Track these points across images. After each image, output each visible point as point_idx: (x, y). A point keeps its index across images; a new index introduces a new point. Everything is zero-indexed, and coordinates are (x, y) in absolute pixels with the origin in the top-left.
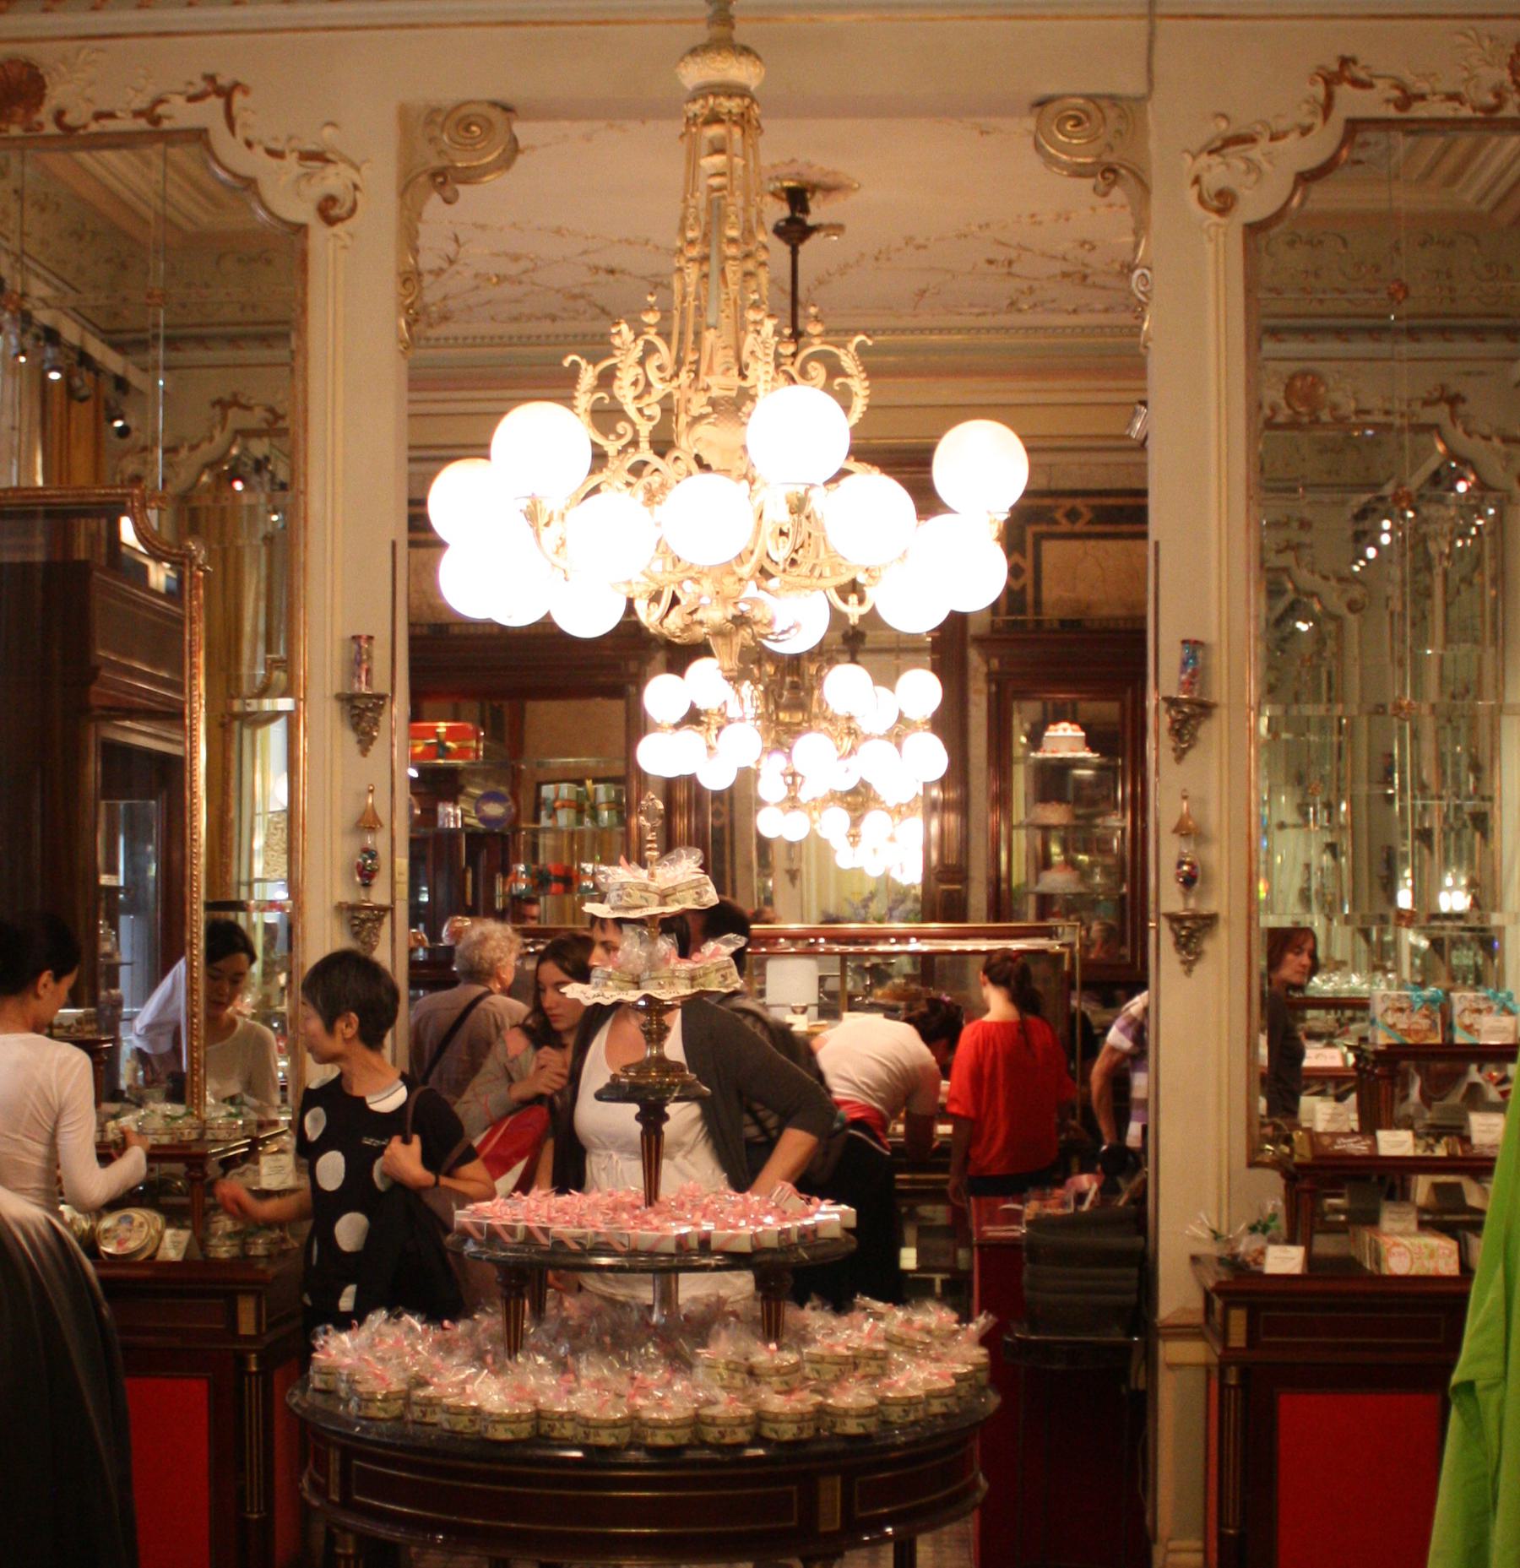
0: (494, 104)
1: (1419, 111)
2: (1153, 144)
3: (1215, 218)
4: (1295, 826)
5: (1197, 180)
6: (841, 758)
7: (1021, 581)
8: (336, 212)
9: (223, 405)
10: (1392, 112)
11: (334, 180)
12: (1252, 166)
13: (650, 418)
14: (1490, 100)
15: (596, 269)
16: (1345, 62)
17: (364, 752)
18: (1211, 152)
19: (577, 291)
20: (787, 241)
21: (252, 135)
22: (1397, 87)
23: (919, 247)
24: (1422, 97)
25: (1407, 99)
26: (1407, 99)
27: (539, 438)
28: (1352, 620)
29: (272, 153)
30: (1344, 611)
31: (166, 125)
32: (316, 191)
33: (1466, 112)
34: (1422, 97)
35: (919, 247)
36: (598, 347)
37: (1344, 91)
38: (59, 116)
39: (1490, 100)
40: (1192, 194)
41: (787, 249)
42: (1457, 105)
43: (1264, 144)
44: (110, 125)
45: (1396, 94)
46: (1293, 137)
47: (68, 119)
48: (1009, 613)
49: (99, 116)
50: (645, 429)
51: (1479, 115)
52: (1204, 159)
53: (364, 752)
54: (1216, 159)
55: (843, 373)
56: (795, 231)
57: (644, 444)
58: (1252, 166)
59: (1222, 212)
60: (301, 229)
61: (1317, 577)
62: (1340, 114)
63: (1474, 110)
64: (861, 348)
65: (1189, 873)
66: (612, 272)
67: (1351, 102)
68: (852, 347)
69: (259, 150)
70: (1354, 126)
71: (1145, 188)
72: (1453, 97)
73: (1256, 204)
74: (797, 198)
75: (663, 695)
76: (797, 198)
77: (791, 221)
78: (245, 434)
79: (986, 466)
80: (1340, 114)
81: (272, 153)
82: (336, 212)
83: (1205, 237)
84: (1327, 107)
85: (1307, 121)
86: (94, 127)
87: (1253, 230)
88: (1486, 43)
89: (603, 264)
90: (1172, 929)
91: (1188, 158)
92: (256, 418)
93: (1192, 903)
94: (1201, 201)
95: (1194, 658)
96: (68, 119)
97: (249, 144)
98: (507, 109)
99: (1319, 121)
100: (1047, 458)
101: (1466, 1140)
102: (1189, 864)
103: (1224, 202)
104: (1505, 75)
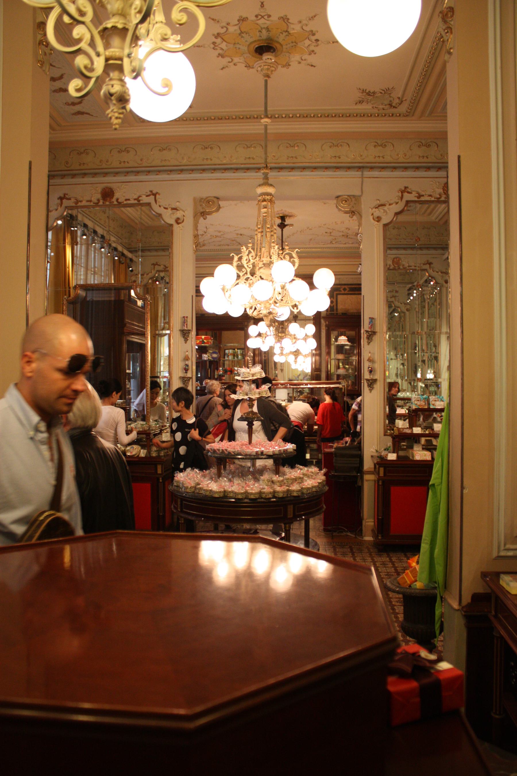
0: (215, 197)
1: (422, 199)
2: (363, 206)
3: (376, 223)
5: (372, 214)
8: (179, 221)
10: (416, 199)
11: (179, 214)
12: (385, 211)
13: (250, 268)
15: (238, 234)
16: (406, 188)
17: (186, 343)
21: (161, 204)
25: (420, 196)
26: (420, 196)
27: (225, 272)
29: (165, 208)
31: (141, 202)
33: (433, 199)
34: (423, 196)
36: (238, 252)
37: (405, 194)
38: (117, 200)
39: (438, 196)
40: (371, 217)
43: (387, 206)
44: (129, 202)
45: (417, 195)
46: (394, 205)
47: (119, 201)
49: (126, 200)
50: (249, 270)
52: (374, 210)
53: (186, 343)
54: (377, 210)
57: (249, 274)
58: (385, 211)
59: (378, 221)
60: (171, 225)
62: (405, 199)
66: (241, 235)
67: (407, 197)
69: (162, 208)
70: (408, 202)
72: (430, 196)
73: (386, 220)
76: (283, 218)
81: (165, 208)
82: (179, 221)
84: (402, 198)
85: (397, 201)
86: (125, 202)
87: (385, 225)
89: (239, 233)
94: (373, 219)
96: (119, 201)
97: (160, 206)
98: (218, 198)
104: (442, 191)
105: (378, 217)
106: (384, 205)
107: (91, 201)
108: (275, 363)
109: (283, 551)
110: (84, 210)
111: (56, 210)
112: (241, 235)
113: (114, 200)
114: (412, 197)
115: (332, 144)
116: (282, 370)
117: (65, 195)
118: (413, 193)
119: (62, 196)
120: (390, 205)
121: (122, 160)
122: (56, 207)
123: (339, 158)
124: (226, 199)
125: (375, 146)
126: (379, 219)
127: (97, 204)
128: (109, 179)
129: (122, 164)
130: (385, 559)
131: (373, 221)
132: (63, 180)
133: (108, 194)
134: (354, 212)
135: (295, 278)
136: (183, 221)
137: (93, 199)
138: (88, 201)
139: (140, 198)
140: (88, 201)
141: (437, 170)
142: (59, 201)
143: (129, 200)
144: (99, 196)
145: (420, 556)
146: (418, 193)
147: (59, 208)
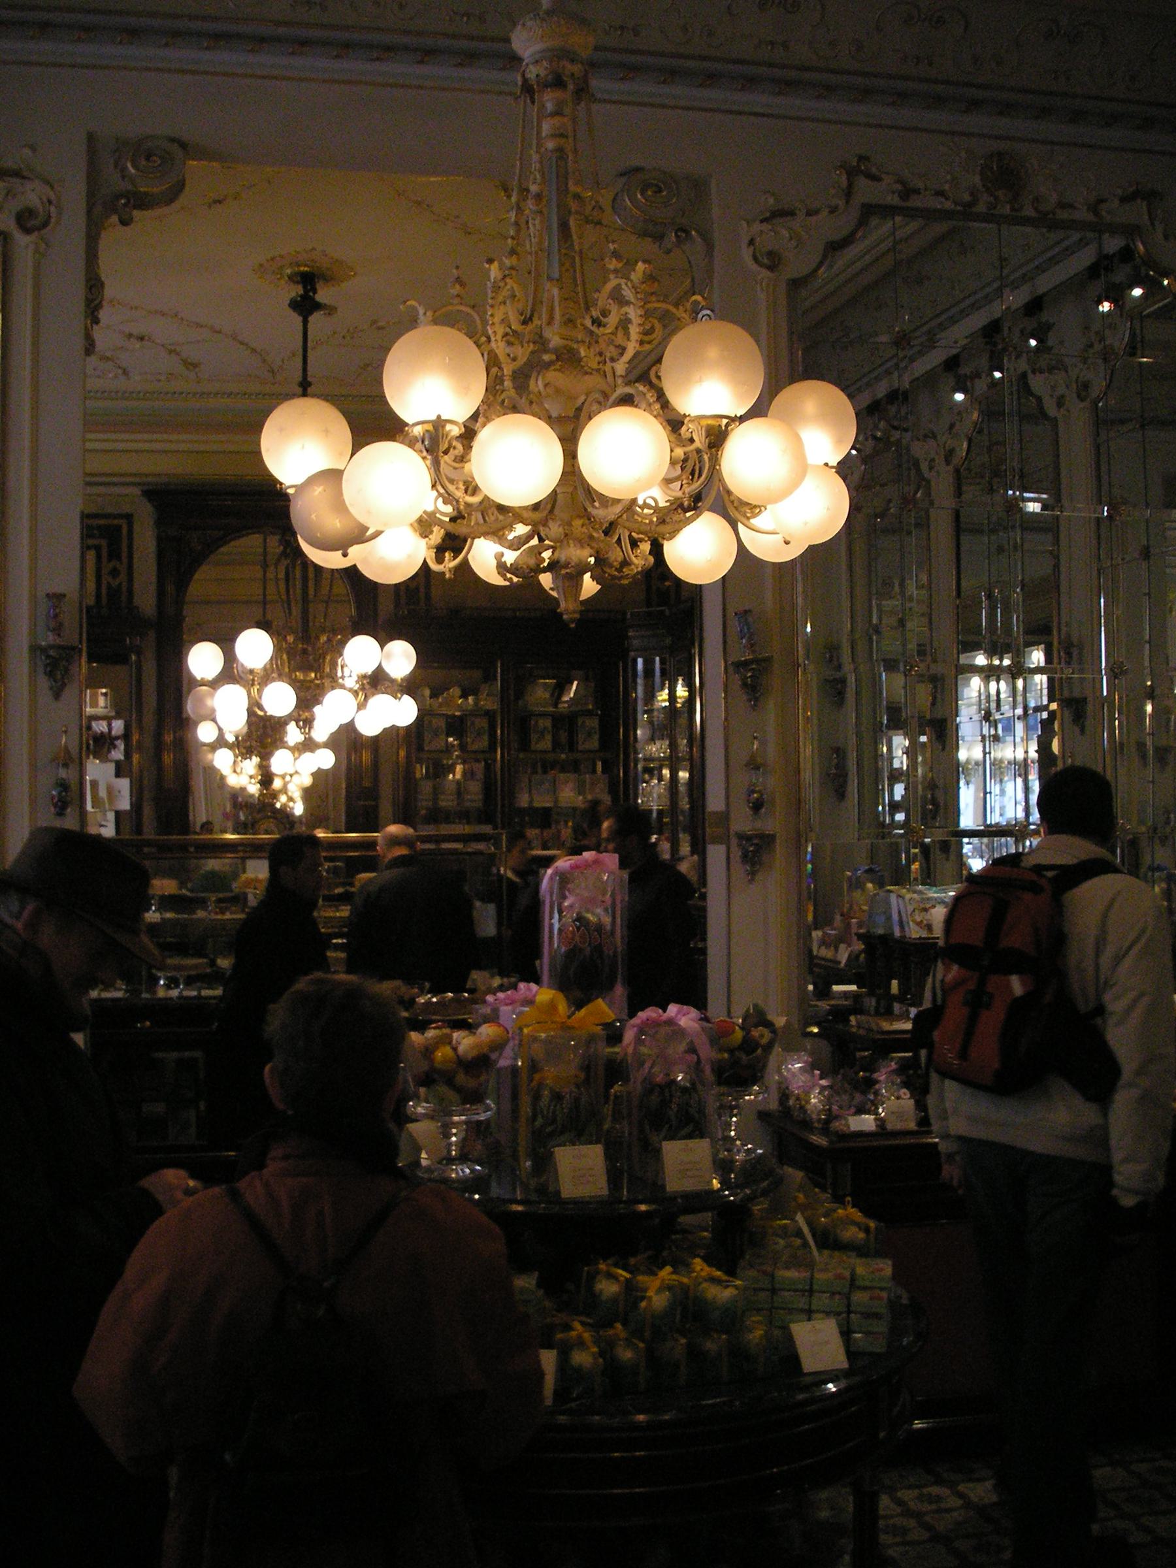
0: (173, 140)
1: (915, 202)
2: (716, 211)
4: (350, 690)
5: (751, 242)
7: (111, 565)
10: (894, 200)
11: (32, 195)
14: (967, 197)
15: (130, 336)
16: (861, 158)
18: (761, 221)
19: (108, 354)
20: (300, 314)
22: (898, 182)
23: (379, 328)
24: (917, 191)
25: (908, 192)
26: (908, 192)
32: (15, 206)
33: (948, 205)
34: (917, 191)
35: (379, 328)
37: (862, 182)
39: (967, 197)
40: (746, 254)
41: (301, 318)
42: (943, 200)
45: (899, 187)
51: (959, 208)
52: (757, 227)
54: (765, 227)
56: (305, 306)
59: (771, 268)
62: (859, 199)
63: (956, 204)
65: (757, 799)
66: (142, 339)
67: (866, 191)
71: (710, 246)
72: (940, 193)
73: (796, 267)
74: (308, 280)
76: (308, 280)
77: (305, 297)
80: (859, 199)
82: (31, 224)
83: (759, 288)
84: (848, 193)
85: (835, 201)
87: (796, 284)
88: (963, 154)
89: (135, 332)
90: (739, 845)
91: (744, 224)
93: (759, 824)
94: (755, 258)
95: (747, 624)
98: (183, 145)
99: (841, 203)
102: (759, 792)
103: (773, 261)
104: (977, 179)
105: (770, 254)
106: (791, 213)
108: (982, 857)
112: (142, 339)
114: (883, 193)
118: (887, 179)
120: (809, 214)
124: (203, 154)
131: (754, 267)
134: (684, 231)
136: (45, 224)
145: (26, 822)
146: (830, 207)
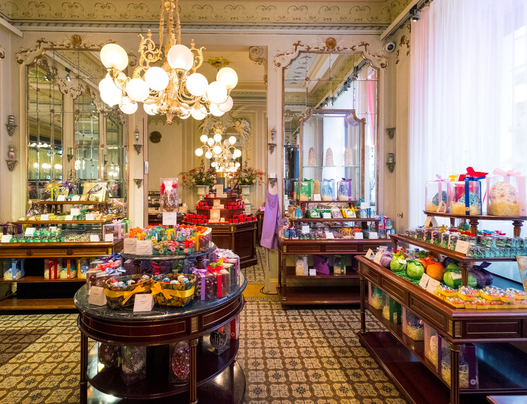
6: (150, 95)
9: (40, 42)
16: (299, 42)
28: (382, 69)
30: (380, 67)
38: (85, 45)
44: (94, 47)
47: (86, 46)
48: (199, 390)
49: (92, 46)
55: (198, 55)
61: (371, 55)
64: (203, 50)
67: (299, 48)
68: (201, 49)
70: (300, 52)
75: (475, 283)
78: (46, 49)
79: (228, 78)
86: (91, 48)
92: (47, 46)
100: (236, 100)
101: (314, 193)
106: (283, 55)
107: (318, 48)
109: (237, 353)
110: (58, 51)
111: (36, 50)
113: (336, 48)
114: (303, 49)
115: (263, 7)
116: (421, 227)
117: (299, 42)
119: (297, 43)
120: (287, 54)
121: (105, 15)
122: (35, 48)
123: (206, 18)
125: (263, 10)
126: (279, 65)
127: (68, 48)
128: (77, 28)
129: (73, 17)
130: (281, 318)
132: (64, 28)
133: (77, 40)
135: (143, 102)
137: (64, 43)
138: (61, 45)
139: (354, 48)
140: (61, 45)
141: (354, 28)
142: (294, 47)
143: (346, 49)
144: (324, 45)
147: (38, 49)
